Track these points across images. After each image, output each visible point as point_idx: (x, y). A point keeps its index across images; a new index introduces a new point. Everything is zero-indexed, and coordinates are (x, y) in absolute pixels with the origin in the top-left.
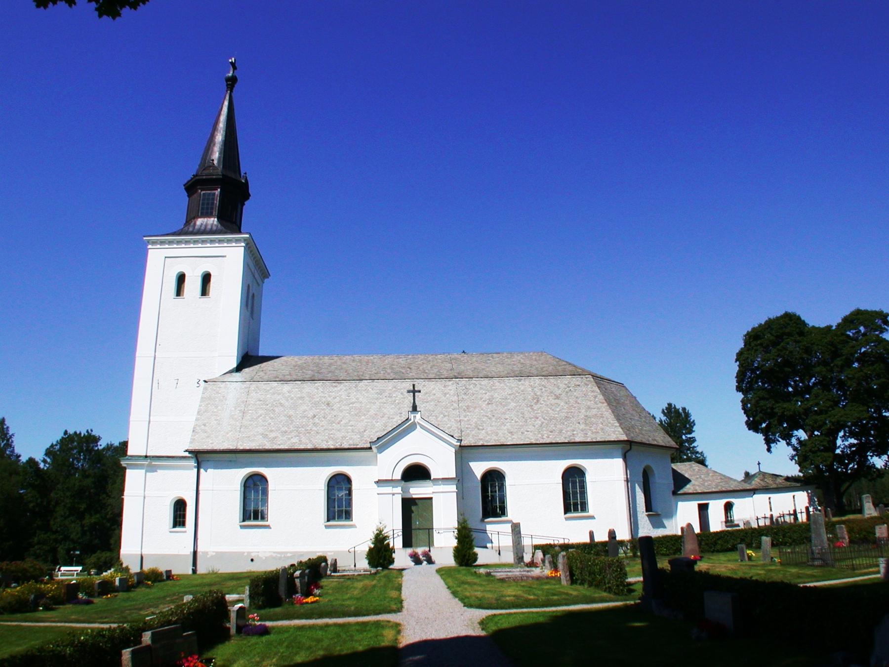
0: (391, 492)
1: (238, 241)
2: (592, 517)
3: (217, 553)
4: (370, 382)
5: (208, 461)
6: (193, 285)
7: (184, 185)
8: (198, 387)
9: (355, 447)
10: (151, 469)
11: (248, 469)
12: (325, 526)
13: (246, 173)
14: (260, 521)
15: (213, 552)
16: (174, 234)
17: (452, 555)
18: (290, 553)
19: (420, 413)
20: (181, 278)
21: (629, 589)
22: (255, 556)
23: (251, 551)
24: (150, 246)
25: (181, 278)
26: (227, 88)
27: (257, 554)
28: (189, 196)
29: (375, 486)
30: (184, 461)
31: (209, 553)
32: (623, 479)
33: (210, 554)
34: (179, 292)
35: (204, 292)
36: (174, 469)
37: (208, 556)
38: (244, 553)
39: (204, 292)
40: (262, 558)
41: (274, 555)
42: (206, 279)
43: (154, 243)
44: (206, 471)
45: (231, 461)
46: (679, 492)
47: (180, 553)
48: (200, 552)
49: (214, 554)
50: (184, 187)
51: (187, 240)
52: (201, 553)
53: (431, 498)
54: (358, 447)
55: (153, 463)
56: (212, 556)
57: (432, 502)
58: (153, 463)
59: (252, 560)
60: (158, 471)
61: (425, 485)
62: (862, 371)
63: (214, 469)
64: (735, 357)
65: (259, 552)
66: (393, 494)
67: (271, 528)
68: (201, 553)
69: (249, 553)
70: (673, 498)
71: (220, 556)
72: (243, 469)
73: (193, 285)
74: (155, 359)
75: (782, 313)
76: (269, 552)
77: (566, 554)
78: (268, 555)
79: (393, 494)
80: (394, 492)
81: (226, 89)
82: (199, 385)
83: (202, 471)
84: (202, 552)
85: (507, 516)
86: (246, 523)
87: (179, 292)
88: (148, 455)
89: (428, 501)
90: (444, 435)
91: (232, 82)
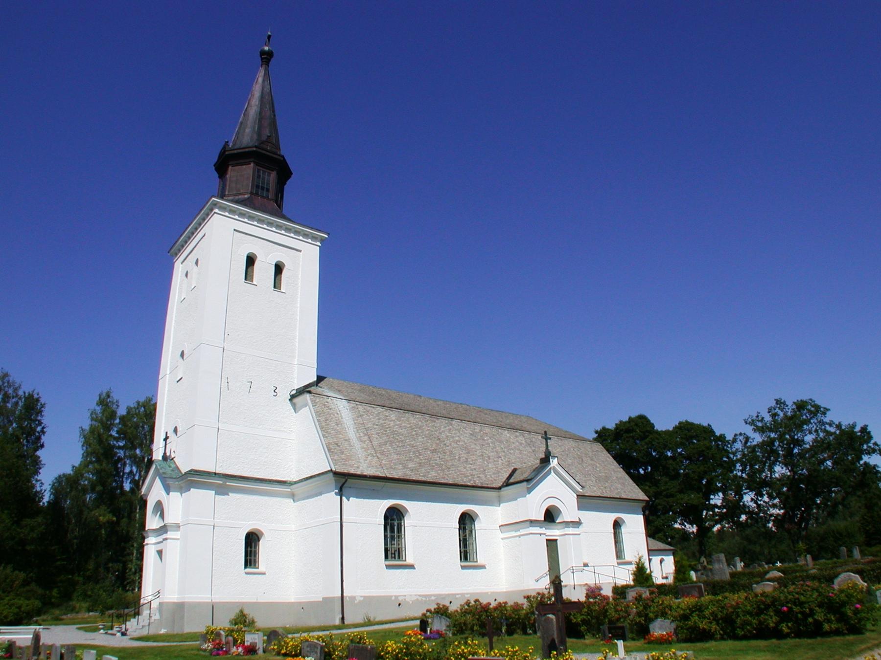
1: (314, 238)
2: (411, 567)
3: (365, 597)
4: (458, 422)
5: (350, 487)
6: (264, 271)
8: (275, 396)
9: (486, 486)
10: (222, 491)
11: (390, 500)
12: (386, 565)
14: (390, 561)
15: (361, 597)
17: (611, 590)
18: (434, 595)
19: (556, 458)
20: (251, 261)
21: (724, 613)
22: (402, 600)
23: (398, 594)
24: (216, 210)
25: (251, 261)
26: (262, 62)
27: (404, 598)
30: (243, 482)
31: (357, 598)
33: (358, 599)
34: (248, 275)
35: (277, 285)
36: (251, 494)
37: (356, 602)
38: (391, 596)
39: (277, 285)
40: (409, 602)
41: (420, 598)
42: (279, 269)
43: (223, 208)
44: (349, 500)
45: (374, 490)
47: (259, 601)
48: (346, 597)
49: (362, 598)
51: (251, 214)
52: (347, 598)
53: (556, 540)
54: (489, 486)
55: (228, 483)
56: (360, 602)
57: (557, 543)
58: (228, 483)
59: (399, 605)
60: (230, 494)
61: (553, 527)
63: (357, 498)
65: (405, 596)
67: (415, 569)
68: (347, 598)
69: (396, 597)
71: (368, 600)
72: (386, 501)
73: (264, 271)
75: (637, 414)
76: (416, 595)
77: (662, 589)
78: (414, 598)
81: (261, 63)
82: (275, 394)
83: (344, 498)
84: (349, 597)
85: (258, 568)
87: (248, 275)
88: (217, 472)
89: (555, 542)
90: (572, 481)
91: (267, 58)
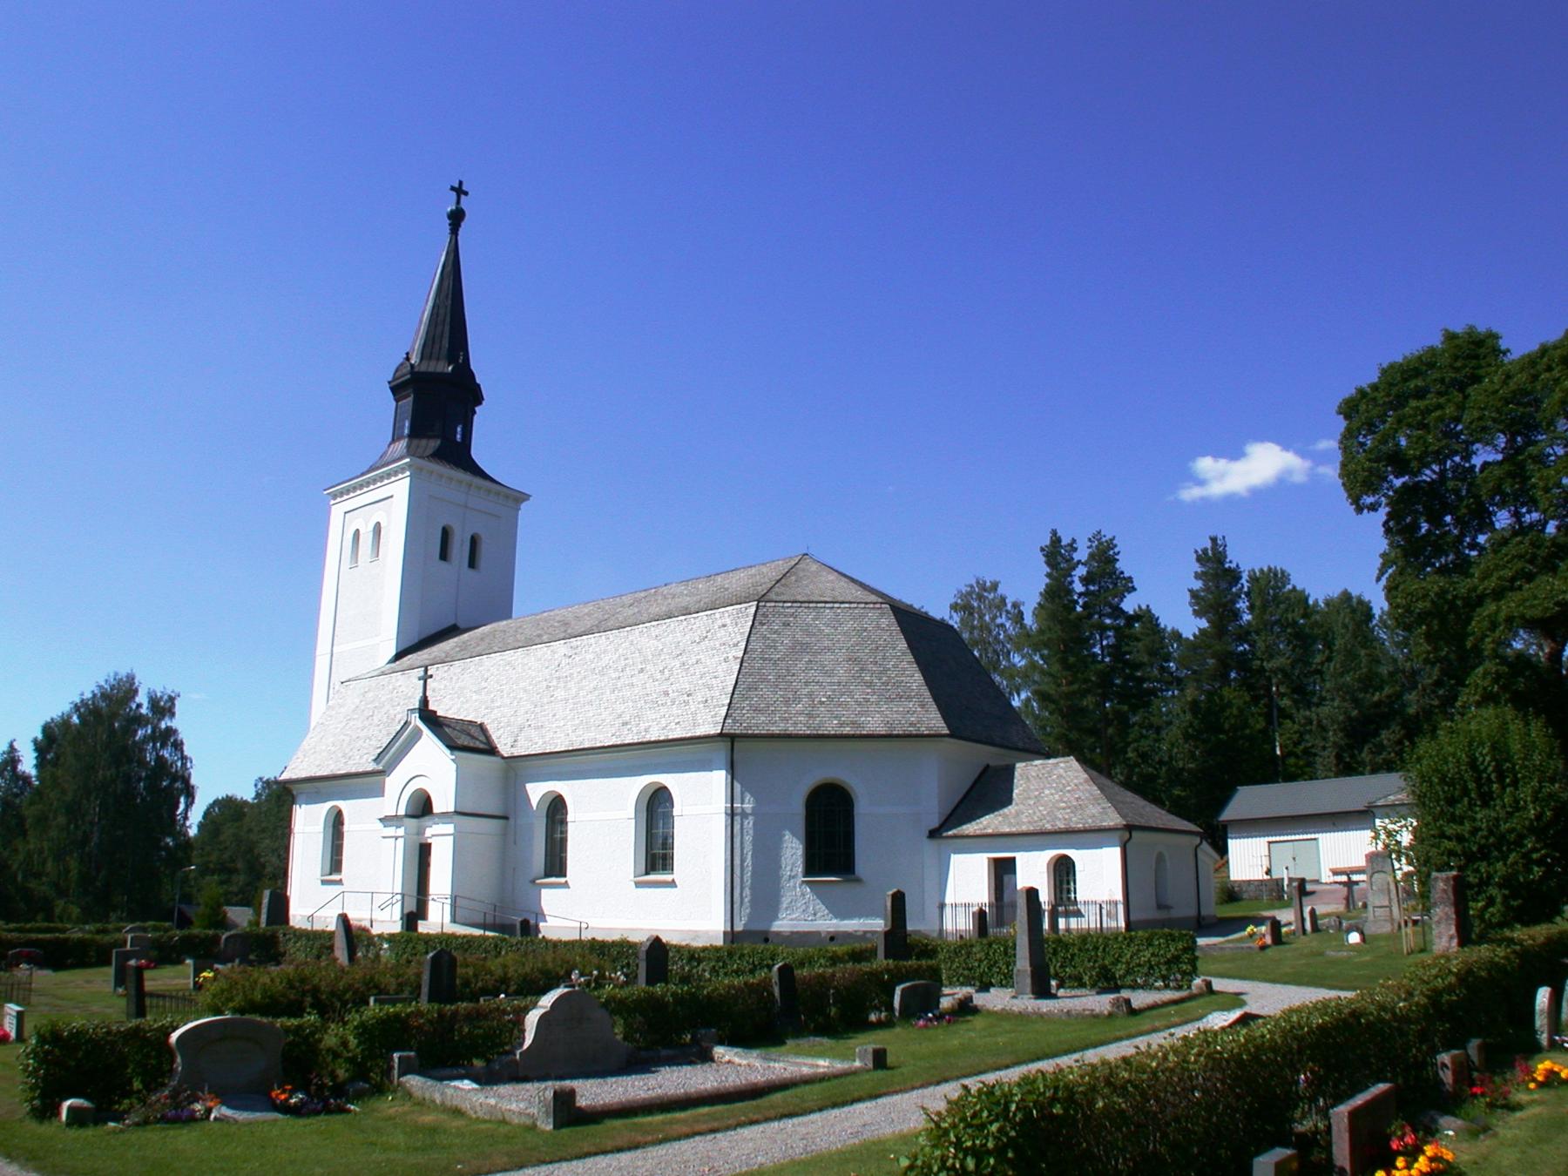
0: (393, 834)
7: (389, 382)
13: (1224, 537)
16: (371, 469)
28: (397, 401)
29: (380, 825)
32: (723, 811)
35: (472, 563)
46: (945, 834)
48: (294, 916)
50: (388, 386)
62: (1496, 655)
64: (1153, 612)
66: (397, 838)
67: (676, 887)
70: (930, 847)
74: (332, 655)
79: (397, 838)
80: (397, 835)
86: (652, 877)
